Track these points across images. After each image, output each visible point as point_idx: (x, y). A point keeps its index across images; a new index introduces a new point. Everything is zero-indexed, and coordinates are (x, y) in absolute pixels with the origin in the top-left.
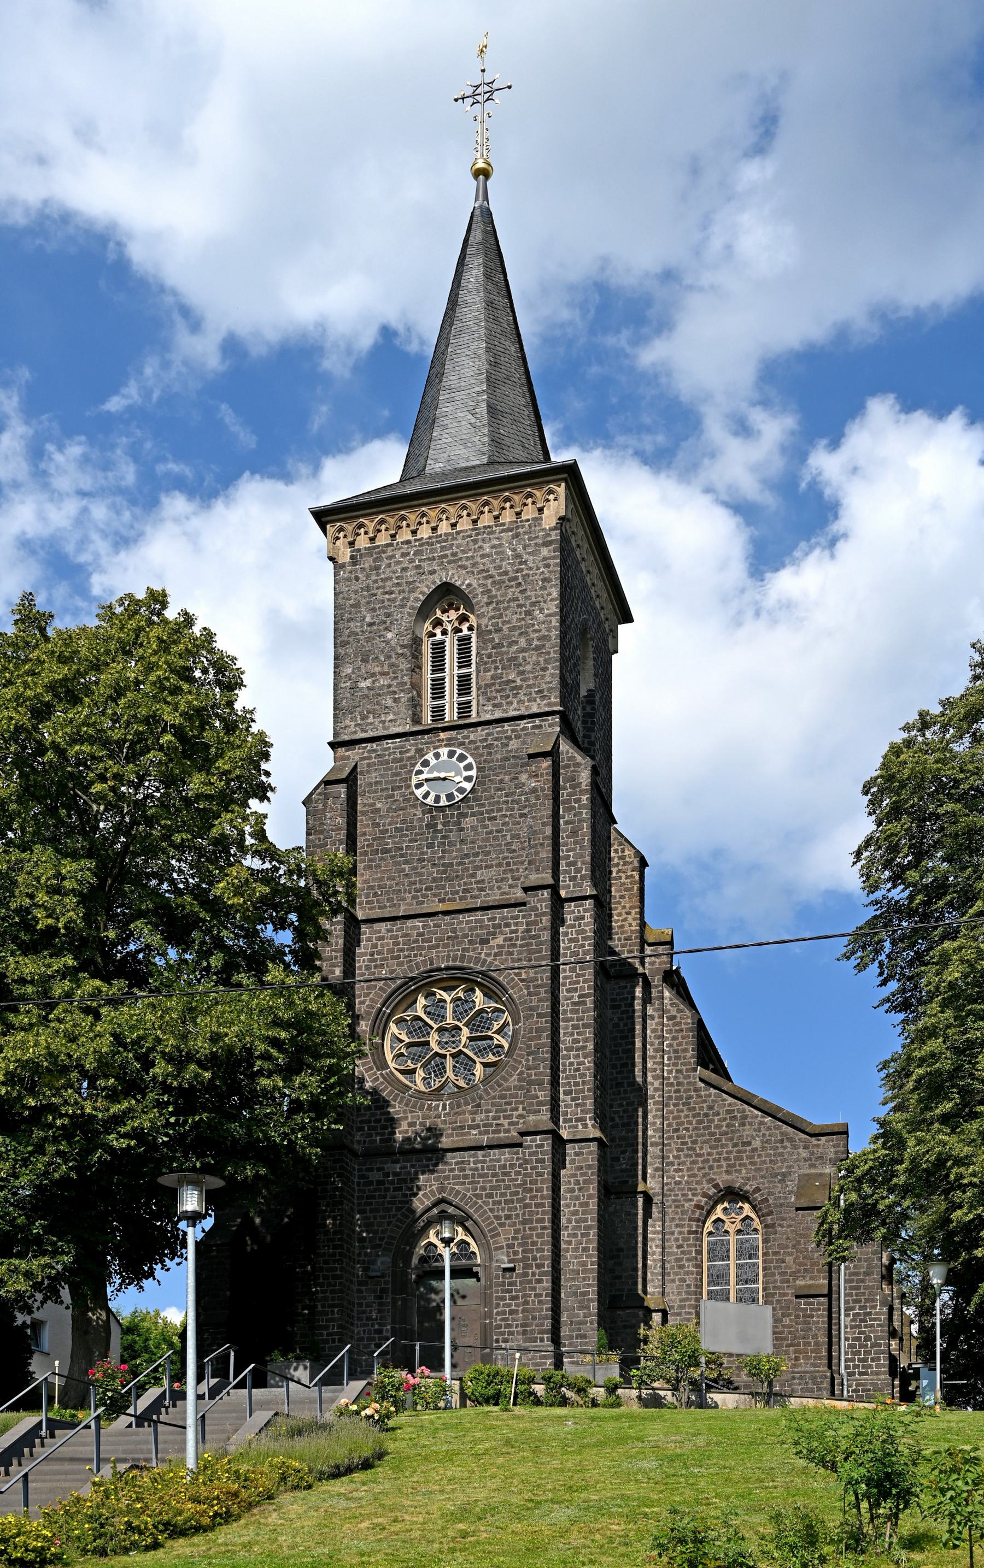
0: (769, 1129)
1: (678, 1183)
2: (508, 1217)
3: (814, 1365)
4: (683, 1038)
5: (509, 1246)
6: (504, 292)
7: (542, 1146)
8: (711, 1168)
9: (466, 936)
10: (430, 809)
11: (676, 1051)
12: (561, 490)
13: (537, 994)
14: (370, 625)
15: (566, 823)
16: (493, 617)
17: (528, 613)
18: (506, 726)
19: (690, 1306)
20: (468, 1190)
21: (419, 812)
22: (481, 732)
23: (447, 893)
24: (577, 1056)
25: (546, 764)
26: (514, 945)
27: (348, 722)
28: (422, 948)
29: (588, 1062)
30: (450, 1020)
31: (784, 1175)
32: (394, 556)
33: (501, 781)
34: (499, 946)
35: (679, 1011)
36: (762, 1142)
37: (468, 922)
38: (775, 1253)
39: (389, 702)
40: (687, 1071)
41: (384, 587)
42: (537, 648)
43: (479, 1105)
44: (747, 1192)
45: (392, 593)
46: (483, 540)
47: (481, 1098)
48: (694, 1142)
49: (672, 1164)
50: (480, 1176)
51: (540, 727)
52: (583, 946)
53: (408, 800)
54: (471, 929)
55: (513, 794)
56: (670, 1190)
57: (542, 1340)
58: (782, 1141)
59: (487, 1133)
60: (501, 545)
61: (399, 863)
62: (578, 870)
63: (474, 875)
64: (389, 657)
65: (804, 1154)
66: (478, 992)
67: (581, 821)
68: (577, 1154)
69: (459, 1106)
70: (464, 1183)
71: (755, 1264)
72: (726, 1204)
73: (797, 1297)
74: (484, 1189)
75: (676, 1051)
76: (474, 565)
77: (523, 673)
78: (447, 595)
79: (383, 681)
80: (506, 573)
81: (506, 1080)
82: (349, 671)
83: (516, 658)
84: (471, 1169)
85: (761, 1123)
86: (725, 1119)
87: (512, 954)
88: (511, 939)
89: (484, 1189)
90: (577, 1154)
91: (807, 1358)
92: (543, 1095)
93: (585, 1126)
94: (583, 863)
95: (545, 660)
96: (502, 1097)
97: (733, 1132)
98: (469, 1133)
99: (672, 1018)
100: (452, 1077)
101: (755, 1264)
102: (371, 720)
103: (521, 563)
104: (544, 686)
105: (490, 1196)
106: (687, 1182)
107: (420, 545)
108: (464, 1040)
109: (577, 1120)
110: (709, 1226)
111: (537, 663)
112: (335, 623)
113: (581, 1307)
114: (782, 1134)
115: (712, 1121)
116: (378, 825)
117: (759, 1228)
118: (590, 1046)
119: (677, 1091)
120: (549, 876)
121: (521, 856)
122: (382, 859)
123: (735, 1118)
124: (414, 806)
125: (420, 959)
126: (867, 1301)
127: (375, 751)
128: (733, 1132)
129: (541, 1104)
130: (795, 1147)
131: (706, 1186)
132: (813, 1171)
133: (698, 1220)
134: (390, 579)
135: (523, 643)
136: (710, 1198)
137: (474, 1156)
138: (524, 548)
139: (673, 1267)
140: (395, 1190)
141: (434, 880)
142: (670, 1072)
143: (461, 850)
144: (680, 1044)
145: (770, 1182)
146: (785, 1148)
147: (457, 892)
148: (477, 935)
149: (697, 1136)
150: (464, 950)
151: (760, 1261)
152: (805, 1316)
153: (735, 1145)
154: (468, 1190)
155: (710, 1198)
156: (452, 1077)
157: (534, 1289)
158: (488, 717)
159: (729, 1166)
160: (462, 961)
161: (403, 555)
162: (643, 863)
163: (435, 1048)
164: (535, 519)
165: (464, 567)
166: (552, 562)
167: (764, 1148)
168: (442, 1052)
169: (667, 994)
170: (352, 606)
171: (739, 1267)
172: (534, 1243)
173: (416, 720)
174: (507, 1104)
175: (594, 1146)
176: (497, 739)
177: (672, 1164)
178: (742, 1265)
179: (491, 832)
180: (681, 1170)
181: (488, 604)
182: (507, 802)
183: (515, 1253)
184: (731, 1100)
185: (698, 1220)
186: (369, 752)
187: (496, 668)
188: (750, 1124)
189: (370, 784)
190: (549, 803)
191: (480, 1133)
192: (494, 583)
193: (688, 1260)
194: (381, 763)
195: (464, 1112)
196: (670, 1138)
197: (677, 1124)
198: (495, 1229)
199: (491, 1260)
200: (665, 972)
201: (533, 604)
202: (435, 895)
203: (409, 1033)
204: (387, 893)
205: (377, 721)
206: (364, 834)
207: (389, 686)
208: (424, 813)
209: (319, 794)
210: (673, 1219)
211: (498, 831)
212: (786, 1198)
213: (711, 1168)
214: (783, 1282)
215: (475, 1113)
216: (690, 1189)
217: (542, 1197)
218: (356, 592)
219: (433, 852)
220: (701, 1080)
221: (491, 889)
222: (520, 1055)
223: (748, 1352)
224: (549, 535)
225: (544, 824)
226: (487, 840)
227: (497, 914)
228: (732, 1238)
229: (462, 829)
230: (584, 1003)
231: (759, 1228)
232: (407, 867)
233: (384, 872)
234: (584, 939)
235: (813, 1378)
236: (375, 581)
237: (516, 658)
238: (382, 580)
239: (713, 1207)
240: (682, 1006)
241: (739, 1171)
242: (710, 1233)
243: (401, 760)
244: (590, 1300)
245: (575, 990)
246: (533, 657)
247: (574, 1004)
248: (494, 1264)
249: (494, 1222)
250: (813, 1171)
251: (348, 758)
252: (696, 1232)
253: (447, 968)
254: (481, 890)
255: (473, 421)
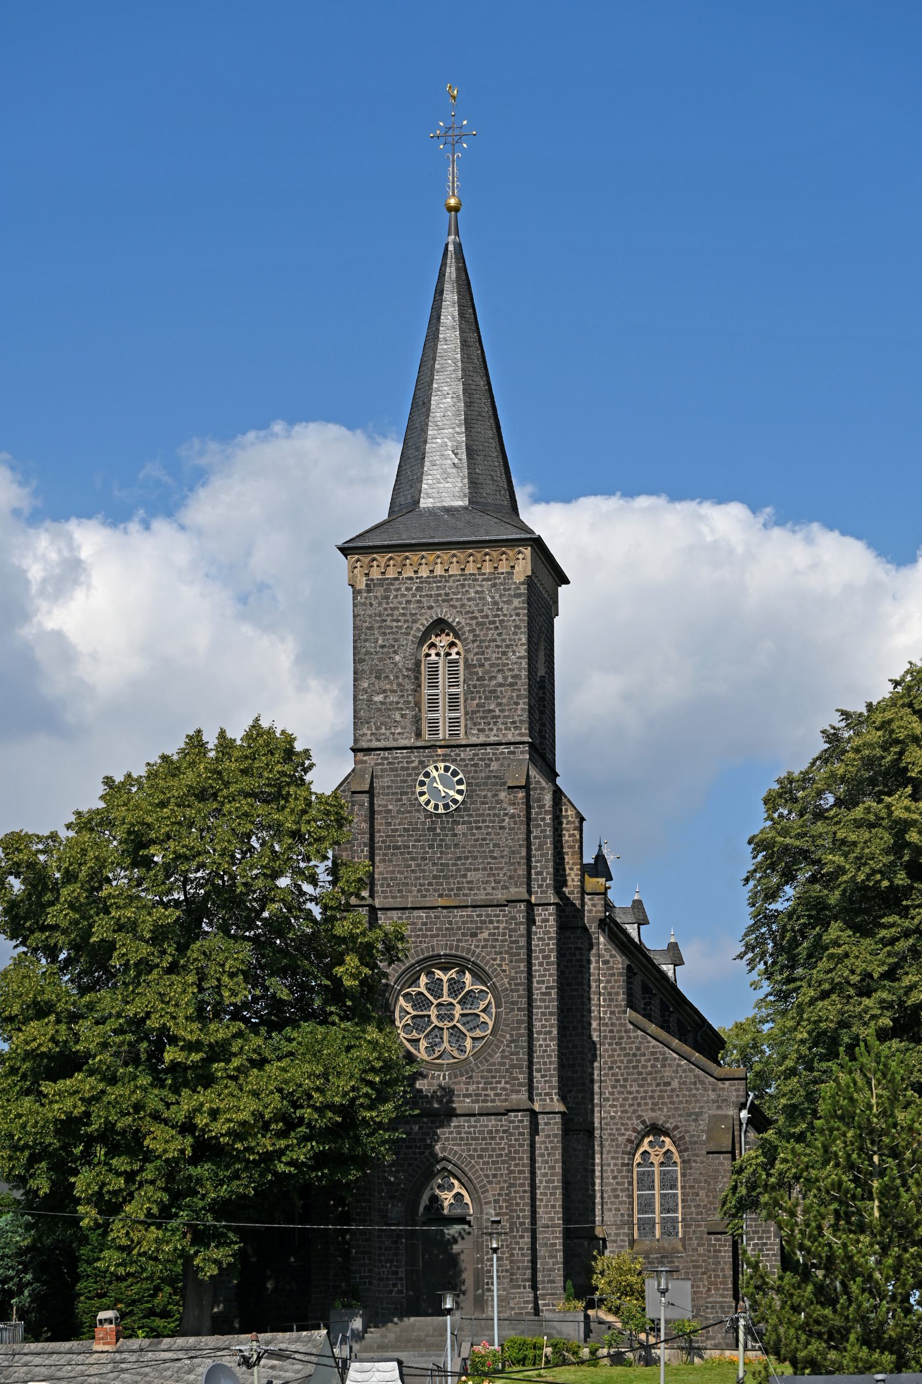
0: (684, 1071)
1: (613, 1118)
2: (495, 1176)
3: (723, 1296)
4: (616, 981)
5: (497, 1201)
6: (473, 327)
7: (522, 1121)
8: (639, 1105)
9: (459, 929)
10: (430, 815)
11: (610, 994)
12: (528, 551)
13: (517, 991)
14: (382, 647)
15: (535, 838)
16: (476, 654)
17: (504, 653)
18: (489, 750)
19: (624, 1234)
20: (463, 1151)
21: (422, 816)
22: (469, 752)
23: (444, 890)
24: (545, 1040)
25: (521, 794)
26: (497, 940)
27: (365, 731)
28: (425, 936)
29: (553, 1045)
30: (446, 998)
31: (697, 1114)
32: (399, 589)
33: (485, 796)
34: (486, 940)
35: (612, 956)
36: (680, 1083)
37: (462, 916)
38: (692, 1187)
39: (398, 718)
40: (619, 1012)
41: (392, 615)
42: (511, 685)
43: (471, 1077)
44: (668, 1129)
45: (398, 621)
46: (469, 585)
47: (472, 1071)
48: (626, 1080)
49: (607, 1099)
50: (473, 1139)
51: (513, 753)
52: (548, 945)
53: (414, 805)
54: (464, 923)
55: (494, 808)
56: (607, 1124)
57: (524, 1287)
58: (695, 1083)
59: (477, 1101)
60: (483, 592)
61: (405, 860)
62: (544, 880)
63: (465, 876)
64: (397, 677)
65: (713, 1096)
66: (467, 974)
67: (545, 837)
68: (546, 1124)
69: (456, 1077)
70: (460, 1145)
71: (675, 1195)
72: (651, 1138)
73: (709, 1233)
74: (475, 1150)
75: (610, 994)
76: (463, 606)
77: (499, 704)
78: (440, 626)
79: (393, 698)
80: (487, 616)
81: (492, 1056)
82: (366, 685)
83: (494, 691)
84: (466, 1133)
85: (679, 1065)
86: (650, 1060)
87: (495, 947)
88: (494, 934)
89: (475, 1150)
90: (546, 1124)
91: (717, 1289)
92: (523, 1078)
93: (552, 1100)
94: (548, 873)
95: (518, 696)
96: (490, 1071)
97: (656, 1072)
98: (464, 1101)
99: (606, 962)
100: (449, 1048)
101: (675, 1195)
102: (383, 731)
103: (498, 609)
104: (516, 718)
105: (480, 1157)
106: (620, 1118)
107: (421, 583)
108: (457, 1016)
109: (546, 1094)
110: (638, 1158)
111: (511, 698)
112: (355, 641)
113: (551, 1257)
114: (695, 1076)
115: (639, 1061)
116: (390, 824)
117: (678, 1161)
118: (555, 1032)
119: (611, 1031)
120: (525, 890)
121: (500, 863)
122: (393, 854)
123: (656, 1059)
124: (418, 811)
125: (424, 945)
126: (763, 1232)
127: (387, 758)
128: (656, 1072)
129: (520, 1085)
130: (706, 1090)
131: (635, 1122)
132: (720, 1112)
133: (629, 1153)
134: (397, 608)
135: (500, 678)
136: (638, 1133)
137: (468, 1121)
138: (500, 597)
139: (609, 1197)
140: (407, 1147)
141: (435, 877)
142: (605, 1013)
143: (455, 853)
144: (612, 987)
145: (686, 1121)
146: (698, 1089)
147: (452, 890)
148: (469, 929)
149: (628, 1074)
150: (458, 941)
151: (679, 1192)
152: (715, 1251)
153: (658, 1085)
154: (463, 1151)
155: (638, 1133)
156: (449, 1048)
157: (518, 1243)
158: (474, 740)
159: (653, 1104)
160: (457, 950)
161: (408, 589)
162: (582, 819)
163: (436, 1022)
164: (508, 573)
165: (454, 607)
166: (521, 611)
167: (681, 1089)
168: (440, 1025)
169: (602, 939)
170: (367, 628)
171: (663, 1196)
172: (518, 1204)
173: (418, 735)
174: (493, 1077)
175: (558, 1118)
176: (481, 759)
177: (607, 1099)
178: (665, 1195)
179: (477, 840)
180: (615, 1106)
181: (473, 641)
182: (489, 815)
183: (501, 1208)
184: (654, 1042)
185: (629, 1153)
186: (383, 758)
187: (480, 698)
188: (670, 1066)
189: (383, 788)
190: (523, 827)
191: (473, 1102)
192: (477, 624)
193: (622, 1190)
194: (392, 770)
195: (459, 1083)
196: (606, 1075)
197: (612, 1062)
198: (484, 1186)
199: (482, 1213)
200: (601, 920)
201: (508, 646)
202: (435, 890)
203: (414, 1007)
204: (398, 884)
205: (388, 732)
206: (379, 831)
207: (398, 703)
208: (426, 817)
209: (344, 791)
210: (609, 1152)
211: (484, 839)
212: (699, 1136)
213: (639, 1105)
214: (697, 1214)
215: (468, 1083)
216: (622, 1124)
217: (523, 1165)
218: (370, 616)
219: (434, 853)
220: (631, 1022)
221: (478, 889)
222: (502, 1036)
223: (676, 1317)
224: (519, 588)
225: (520, 846)
226: (475, 846)
227: (483, 911)
228: (656, 1169)
229: (455, 835)
230: (550, 994)
231: (678, 1161)
232: (413, 863)
233: (395, 866)
234: (549, 939)
235: (722, 1308)
236: (386, 609)
237: (494, 691)
238: (392, 609)
239: (642, 1140)
240: (614, 952)
241: (661, 1109)
242: (639, 1164)
243: (407, 769)
244: (557, 1250)
245: (543, 982)
246: (507, 692)
247: (542, 994)
248: (485, 1217)
249: (486, 1182)
250: (720, 1112)
251: (365, 762)
252: (628, 1164)
253: (445, 955)
254: (471, 889)
255: (456, 461)
